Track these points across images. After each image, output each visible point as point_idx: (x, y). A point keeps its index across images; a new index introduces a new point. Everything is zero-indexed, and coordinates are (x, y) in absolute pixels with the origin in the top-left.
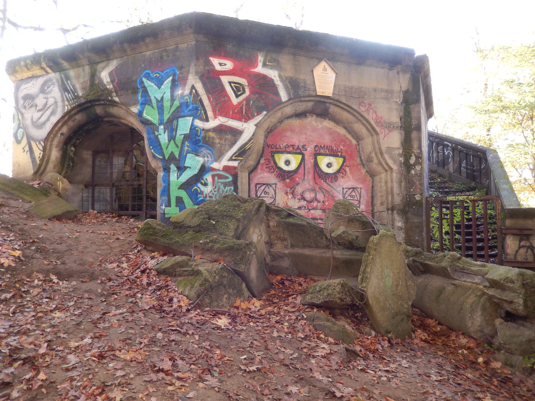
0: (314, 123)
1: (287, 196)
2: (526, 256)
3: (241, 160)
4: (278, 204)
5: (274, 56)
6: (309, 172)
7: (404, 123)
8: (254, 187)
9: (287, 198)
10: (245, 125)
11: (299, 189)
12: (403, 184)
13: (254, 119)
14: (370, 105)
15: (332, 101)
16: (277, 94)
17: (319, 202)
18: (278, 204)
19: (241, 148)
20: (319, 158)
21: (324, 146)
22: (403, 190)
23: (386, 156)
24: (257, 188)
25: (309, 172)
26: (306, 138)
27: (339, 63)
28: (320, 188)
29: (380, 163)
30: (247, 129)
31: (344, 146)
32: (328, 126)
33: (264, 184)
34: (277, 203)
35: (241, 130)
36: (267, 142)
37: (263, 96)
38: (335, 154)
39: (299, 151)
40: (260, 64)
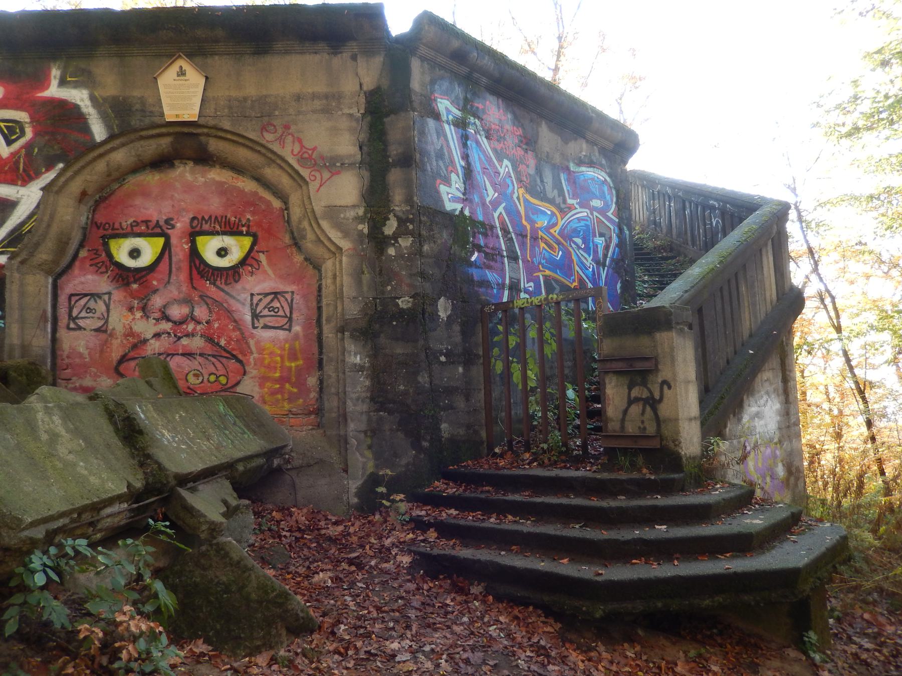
0: (189, 177)
1: (133, 314)
2: (643, 422)
3: (12, 252)
4: (114, 329)
5: (82, 64)
6: (179, 269)
7: (369, 154)
8: (67, 300)
9: (132, 317)
10: (23, 191)
11: (157, 301)
12: (366, 277)
13: (41, 179)
14: (287, 127)
15: (205, 130)
16: (86, 129)
17: (199, 323)
18: (114, 329)
19: (12, 232)
20: (200, 240)
21: (210, 217)
22: (365, 289)
23: (325, 224)
24: (73, 303)
25: (179, 269)
26: (173, 206)
27: (217, 57)
28: (201, 296)
29: (319, 240)
30: (25, 197)
31: (253, 213)
32: (218, 178)
33: (86, 295)
34: (110, 327)
35: (15, 200)
36: (96, 220)
37: (59, 137)
38: (235, 229)
39: (158, 230)
40: (54, 83)
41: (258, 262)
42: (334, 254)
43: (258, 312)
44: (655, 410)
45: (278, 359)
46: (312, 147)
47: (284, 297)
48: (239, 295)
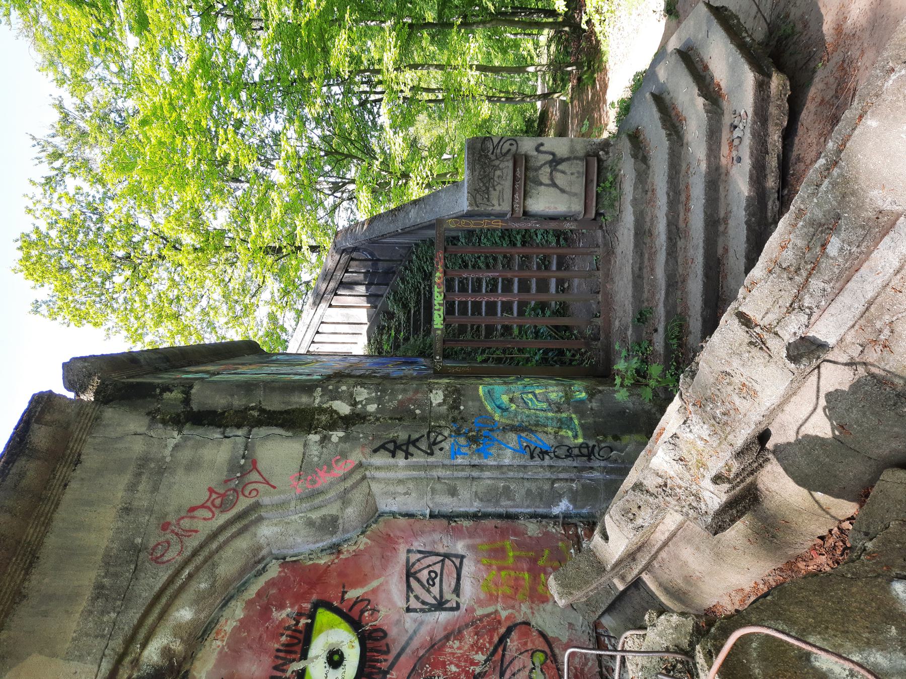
38: (301, 636)
41: (358, 601)
42: (364, 478)
43: (434, 602)
44: (562, 160)
45: (503, 573)
46: (208, 493)
47: (414, 564)
48: (407, 631)
